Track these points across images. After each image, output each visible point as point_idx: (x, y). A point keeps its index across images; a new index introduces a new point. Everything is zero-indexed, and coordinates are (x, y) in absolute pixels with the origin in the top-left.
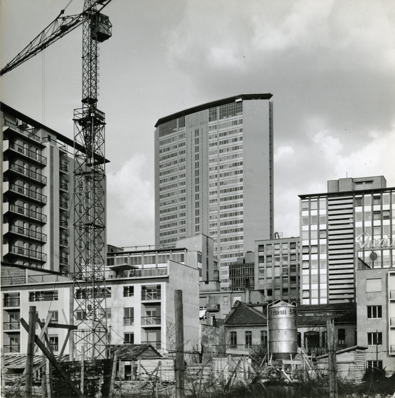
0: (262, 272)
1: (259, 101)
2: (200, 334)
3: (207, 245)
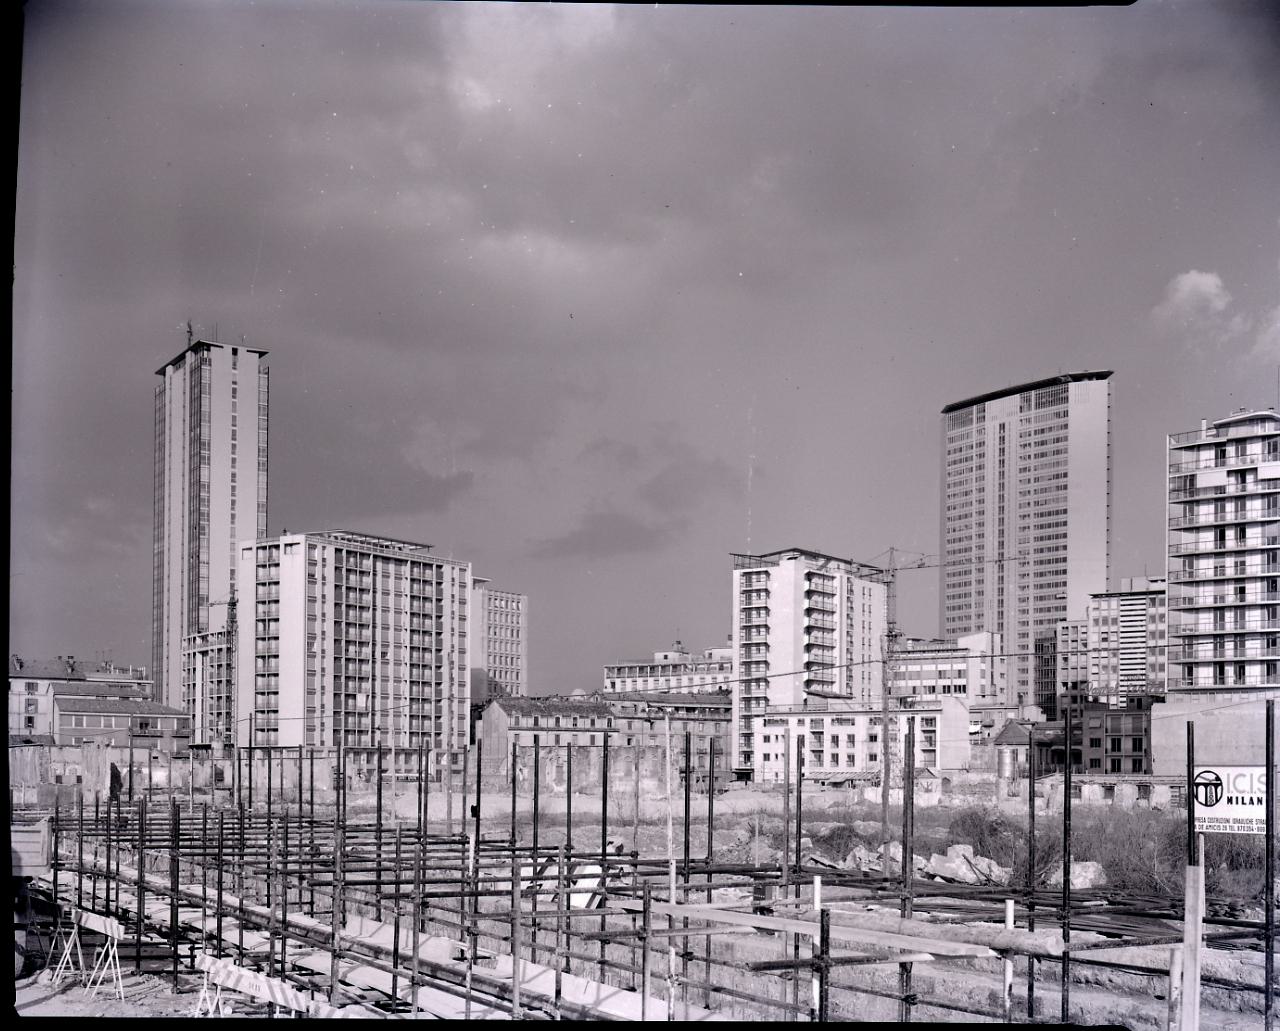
0: (1066, 659)
1: (1095, 383)
2: (969, 753)
3: (993, 642)
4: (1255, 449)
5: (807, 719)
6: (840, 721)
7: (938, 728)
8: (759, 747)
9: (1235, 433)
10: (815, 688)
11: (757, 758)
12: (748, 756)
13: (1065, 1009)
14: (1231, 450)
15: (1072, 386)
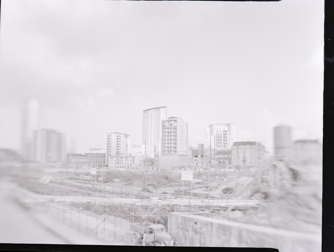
4: (173, 122)
5: (116, 158)
6: (121, 158)
7: (135, 159)
8: (109, 162)
9: (171, 119)
10: (118, 153)
11: (109, 163)
12: (108, 163)
13: (122, 192)
14: (170, 122)
15: (161, 108)
